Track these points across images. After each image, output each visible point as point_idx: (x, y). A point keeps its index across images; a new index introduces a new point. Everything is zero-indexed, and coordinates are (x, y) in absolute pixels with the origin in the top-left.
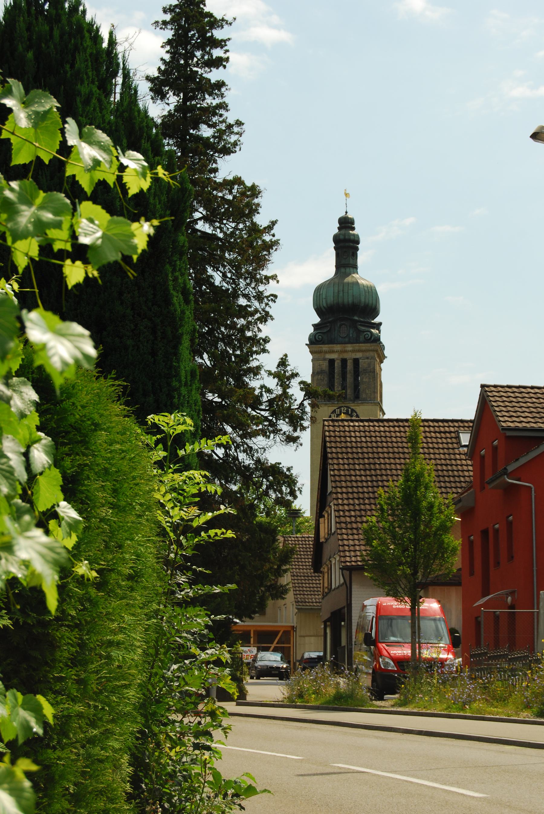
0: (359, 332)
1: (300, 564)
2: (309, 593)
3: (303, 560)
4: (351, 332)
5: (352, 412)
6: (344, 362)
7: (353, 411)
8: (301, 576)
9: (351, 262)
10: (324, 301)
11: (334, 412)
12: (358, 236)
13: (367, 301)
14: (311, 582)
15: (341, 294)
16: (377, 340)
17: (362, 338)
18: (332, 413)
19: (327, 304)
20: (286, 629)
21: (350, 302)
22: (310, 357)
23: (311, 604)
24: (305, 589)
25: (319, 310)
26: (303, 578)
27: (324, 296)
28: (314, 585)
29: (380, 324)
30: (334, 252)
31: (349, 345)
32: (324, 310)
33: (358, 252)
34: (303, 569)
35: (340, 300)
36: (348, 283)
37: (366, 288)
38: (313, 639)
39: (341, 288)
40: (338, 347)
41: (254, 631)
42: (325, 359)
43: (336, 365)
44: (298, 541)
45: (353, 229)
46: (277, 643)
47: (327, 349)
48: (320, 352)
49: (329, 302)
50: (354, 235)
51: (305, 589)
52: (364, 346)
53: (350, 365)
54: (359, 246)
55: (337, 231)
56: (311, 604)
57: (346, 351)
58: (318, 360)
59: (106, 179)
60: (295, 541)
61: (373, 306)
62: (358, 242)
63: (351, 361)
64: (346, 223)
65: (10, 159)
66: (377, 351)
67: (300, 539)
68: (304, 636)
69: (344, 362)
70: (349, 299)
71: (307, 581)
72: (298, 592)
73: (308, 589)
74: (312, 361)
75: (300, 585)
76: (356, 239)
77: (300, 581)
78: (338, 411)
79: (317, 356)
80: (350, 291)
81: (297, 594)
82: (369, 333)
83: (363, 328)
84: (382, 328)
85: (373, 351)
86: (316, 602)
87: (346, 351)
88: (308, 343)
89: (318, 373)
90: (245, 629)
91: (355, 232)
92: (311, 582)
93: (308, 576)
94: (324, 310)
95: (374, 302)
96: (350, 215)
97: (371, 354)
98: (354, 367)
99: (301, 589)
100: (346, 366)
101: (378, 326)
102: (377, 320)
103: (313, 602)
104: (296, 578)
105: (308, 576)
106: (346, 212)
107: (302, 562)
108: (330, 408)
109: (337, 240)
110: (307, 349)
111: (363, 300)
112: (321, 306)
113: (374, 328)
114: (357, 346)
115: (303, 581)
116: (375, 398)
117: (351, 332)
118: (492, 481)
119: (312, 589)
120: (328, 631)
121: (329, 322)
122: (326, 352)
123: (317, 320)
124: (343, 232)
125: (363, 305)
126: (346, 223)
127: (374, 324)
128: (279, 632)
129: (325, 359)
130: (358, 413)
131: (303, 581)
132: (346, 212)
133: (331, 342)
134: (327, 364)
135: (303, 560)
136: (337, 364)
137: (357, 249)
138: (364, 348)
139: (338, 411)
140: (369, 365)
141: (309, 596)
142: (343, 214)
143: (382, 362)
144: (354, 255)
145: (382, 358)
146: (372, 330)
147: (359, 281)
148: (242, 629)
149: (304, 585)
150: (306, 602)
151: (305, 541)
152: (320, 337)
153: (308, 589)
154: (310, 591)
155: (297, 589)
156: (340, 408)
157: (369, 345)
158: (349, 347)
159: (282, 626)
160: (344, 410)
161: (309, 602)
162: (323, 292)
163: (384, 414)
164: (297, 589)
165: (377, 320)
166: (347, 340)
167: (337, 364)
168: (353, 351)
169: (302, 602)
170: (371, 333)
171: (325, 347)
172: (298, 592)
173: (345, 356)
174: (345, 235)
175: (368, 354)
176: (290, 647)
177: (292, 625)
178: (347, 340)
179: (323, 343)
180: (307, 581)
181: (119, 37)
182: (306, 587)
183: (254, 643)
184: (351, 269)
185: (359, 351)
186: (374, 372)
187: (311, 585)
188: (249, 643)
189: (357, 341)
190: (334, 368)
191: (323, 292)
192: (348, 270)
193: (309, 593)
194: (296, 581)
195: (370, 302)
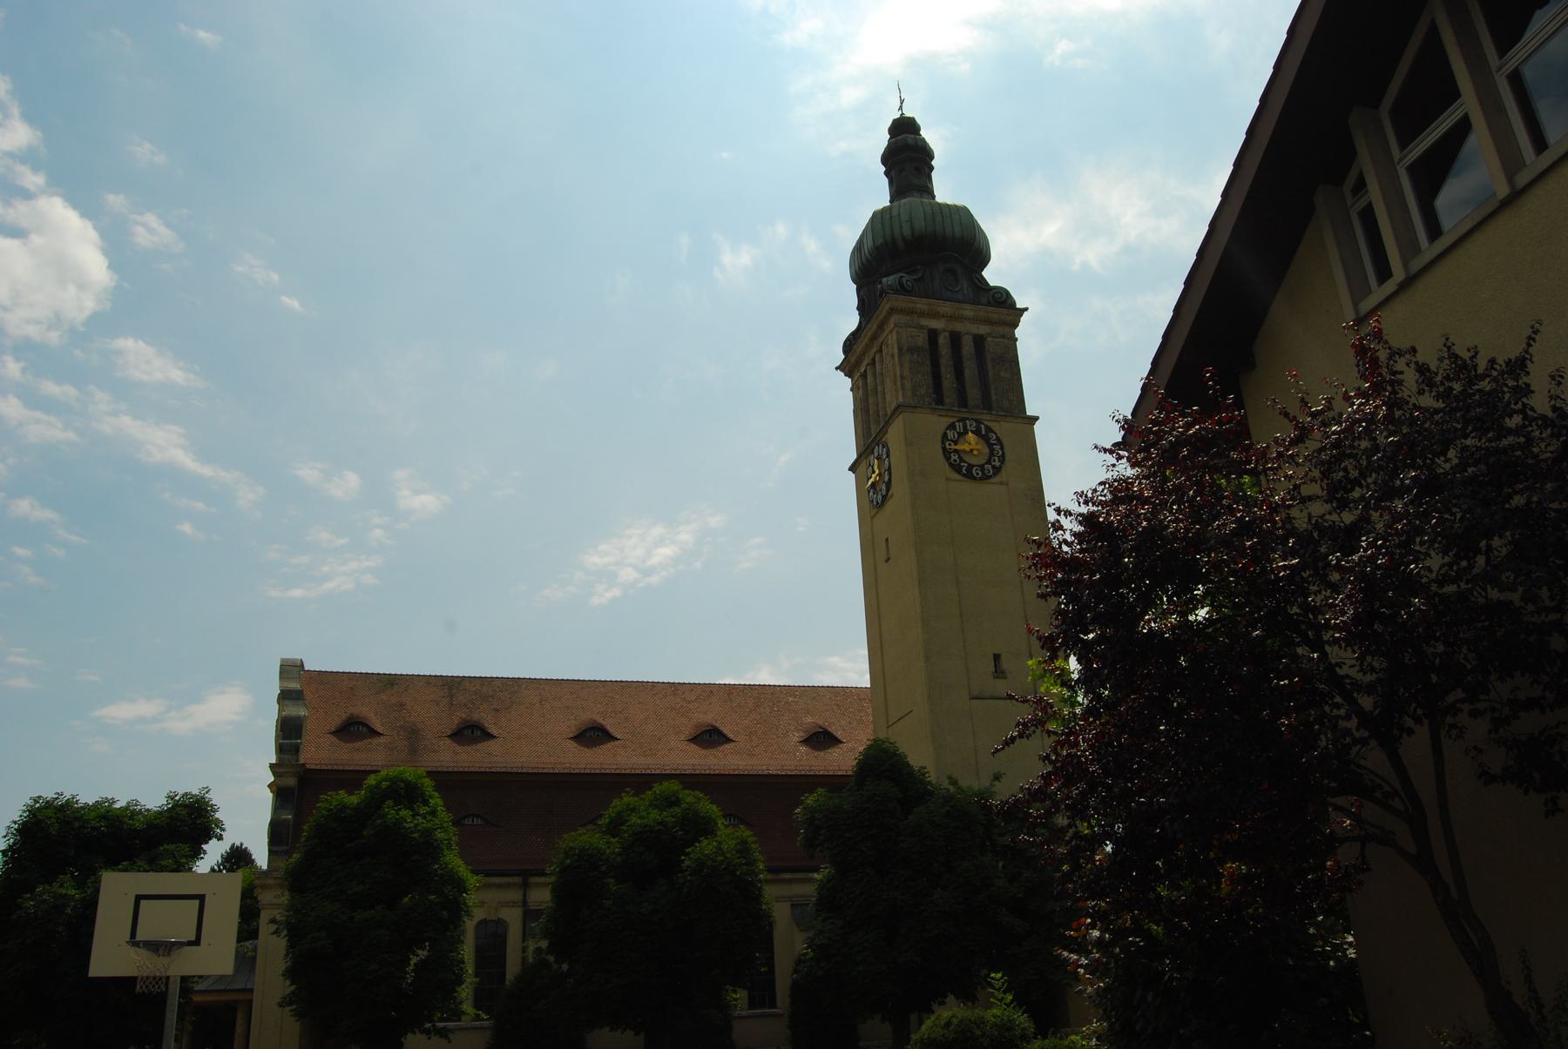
7: (989, 429)
11: (952, 426)
21: (958, 234)
22: (1018, 332)
40: (945, 308)
42: (922, 327)
53: (968, 348)
57: (961, 319)
87: (961, 319)
118: (1401, 160)
122: (922, 314)
156: (963, 420)
160: (971, 425)
163: (190, 821)
167: (943, 340)
168: (973, 320)
171: (922, 304)
173: (958, 327)
185: (991, 323)
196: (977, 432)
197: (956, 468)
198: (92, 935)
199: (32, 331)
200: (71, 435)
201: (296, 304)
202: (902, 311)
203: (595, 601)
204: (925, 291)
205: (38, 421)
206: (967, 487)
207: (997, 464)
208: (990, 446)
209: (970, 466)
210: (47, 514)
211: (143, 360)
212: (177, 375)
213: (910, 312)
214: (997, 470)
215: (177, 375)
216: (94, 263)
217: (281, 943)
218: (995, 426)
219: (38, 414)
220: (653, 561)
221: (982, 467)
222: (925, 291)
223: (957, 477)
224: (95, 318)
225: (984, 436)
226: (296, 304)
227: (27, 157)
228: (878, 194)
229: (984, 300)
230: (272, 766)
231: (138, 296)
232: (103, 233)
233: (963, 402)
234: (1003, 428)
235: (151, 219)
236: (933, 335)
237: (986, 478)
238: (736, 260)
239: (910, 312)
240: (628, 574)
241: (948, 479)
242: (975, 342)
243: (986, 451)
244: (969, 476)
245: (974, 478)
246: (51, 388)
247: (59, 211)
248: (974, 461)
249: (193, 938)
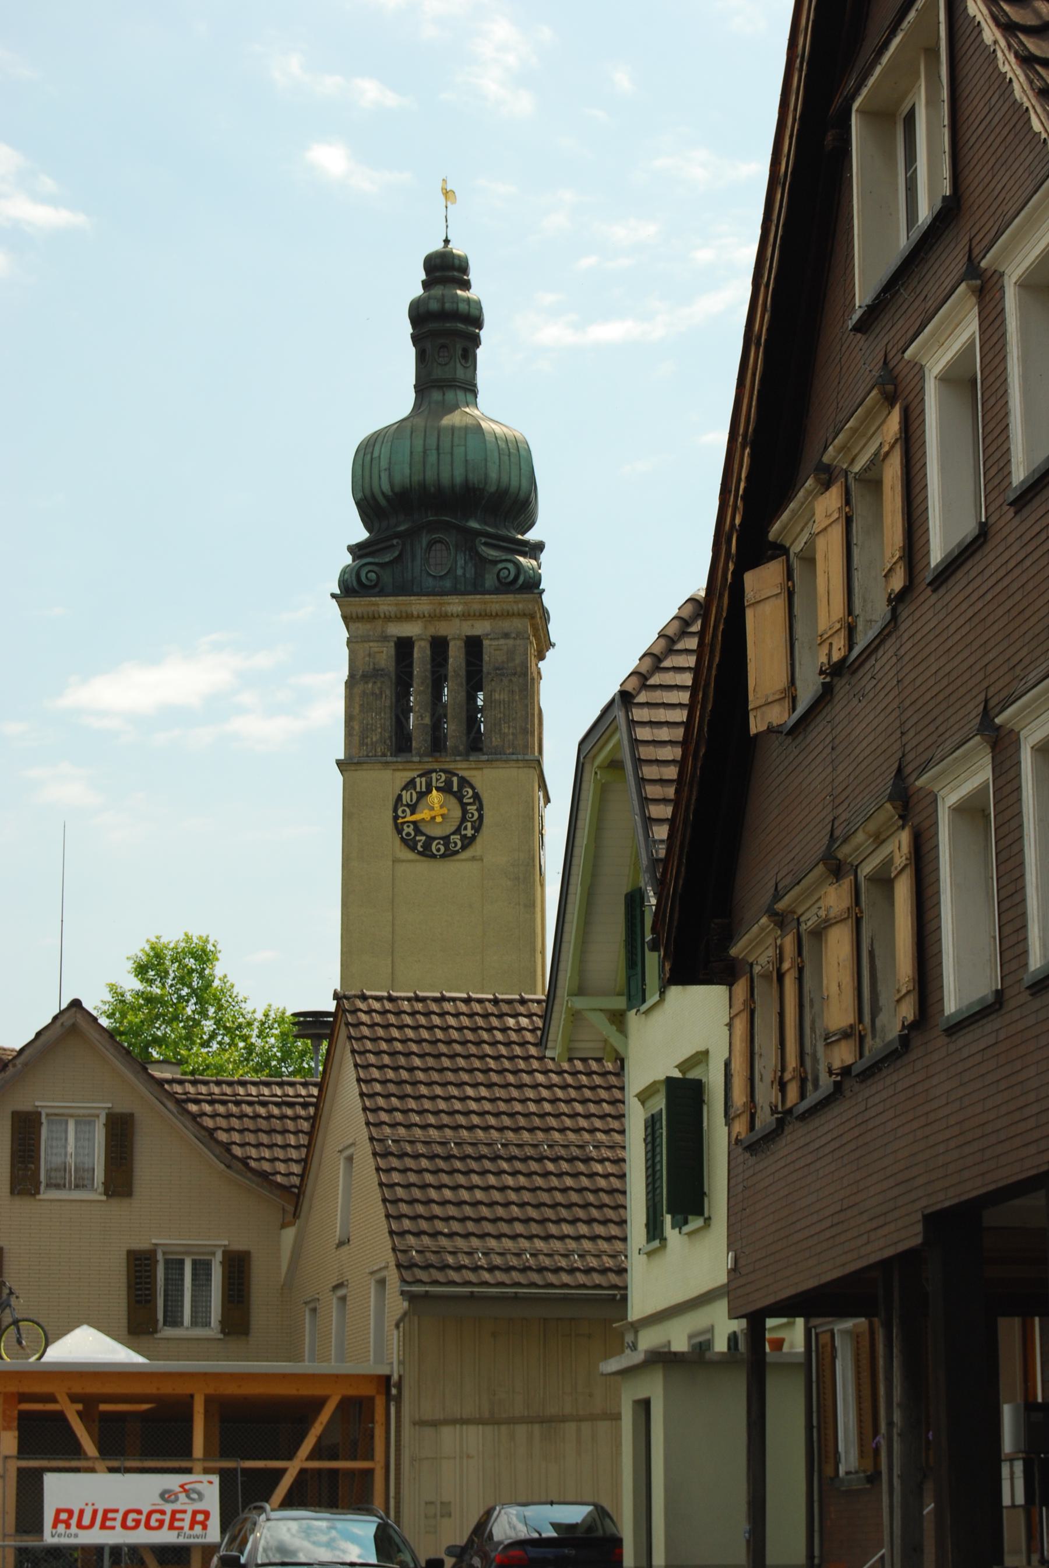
0: (483, 563)
1: (412, 1104)
2: (456, 1227)
3: (423, 1090)
4: (461, 562)
5: (461, 786)
6: (439, 646)
7: (464, 782)
8: (416, 1156)
9: (460, 373)
10: (384, 476)
11: (411, 784)
12: (478, 304)
13: (505, 479)
14: (461, 1179)
15: (432, 458)
16: (532, 585)
17: (490, 580)
18: (405, 788)
19: (392, 490)
20: (351, 1392)
21: (459, 480)
23: (471, 1276)
24: (437, 1210)
25: (369, 507)
26: (424, 1163)
27: (384, 464)
28: (479, 1195)
29: (539, 547)
30: (410, 353)
31: (455, 599)
32: (383, 502)
33: (480, 352)
34: (425, 1127)
35: (430, 475)
36: (453, 429)
37: (502, 445)
38: (473, 1435)
39: (432, 441)
40: (421, 605)
41: (209, 1400)
42: (385, 638)
43: (416, 654)
44: (398, 1013)
45: (466, 285)
46: (311, 1457)
47: (393, 609)
48: (373, 618)
49: (398, 478)
50: (468, 301)
51: (437, 1210)
52: (497, 602)
54: (483, 334)
55: (419, 291)
56: (471, 1276)
57: (445, 617)
58: (365, 639)
60: (384, 1013)
61: (522, 494)
62: (477, 322)
63: (460, 644)
64: (445, 270)
66: (532, 617)
67: (405, 1006)
68: (435, 1424)
69: (439, 646)
70: (452, 472)
71: (445, 1179)
72: (407, 1224)
73: (452, 1211)
74: (349, 642)
75: (417, 1193)
76: (474, 312)
77: (413, 1178)
78: (421, 783)
79: (362, 628)
80: (459, 451)
81: (402, 1234)
82: (510, 566)
83: (493, 553)
84: (544, 557)
85: (522, 615)
86: (492, 1269)
87: (445, 617)
88: (338, 591)
89: (366, 677)
90: (168, 1389)
91: (473, 293)
92: (461, 1179)
93: (448, 1158)
94: (383, 502)
95: (525, 483)
96: (457, 248)
97: (518, 624)
98: (469, 663)
99: (420, 1209)
100: (446, 659)
101: (536, 549)
102: (532, 536)
103: (476, 1269)
104: (395, 1162)
105: (448, 1158)
106: (447, 241)
107: (418, 1098)
108: (398, 774)
109: (421, 316)
110: (334, 610)
111: (493, 475)
112: (376, 490)
113: (524, 554)
114: (476, 602)
115: (429, 1178)
116: (527, 747)
117: (461, 562)
119: (468, 1210)
120: (145, 1407)
121: (398, 535)
122: (388, 619)
123: (361, 534)
124: (437, 291)
125: (492, 489)
126: (445, 270)
127: (526, 543)
128: (317, 1404)
130: (479, 790)
131: (429, 1178)
132: (447, 241)
133: (403, 589)
134: (392, 651)
135: (423, 1090)
136: (421, 653)
137: (476, 341)
138: (495, 608)
139: (421, 783)
140: (511, 653)
141: (460, 1242)
142: (438, 246)
143: (541, 657)
144: (469, 357)
145: (544, 644)
146: (521, 559)
147: (484, 424)
148: (150, 1389)
149: (433, 1194)
150: (446, 1267)
151: (428, 1014)
152: (372, 576)
153: (452, 1211)
154: (463, 1220)
155: (404, 1208)
156: (426, 774)
157: (510, 597)
158: (455, 605)
159: (337, 1378)
160: (438, 779)
161: (459, 1268)
162: (383, 452)
164: (404, 1208)
165: (532, 536)
166: (448, 584)
167: (421, 653)
168: (465, 616)
169: (427, 1267)
170: (518, 566)
171: (386, 605)
172: (407, 1224)
173: (443, 629)
174: (442, 300)
175: (506, 625)
176: (369, 1473)
177: (384, 1370)
178: (448, 584)
179: (382, 593)
180: (445, 1179)
182: (443, 1203)
183: (208, 1455)
184: (461, 395)
185: (484, 615)
186: (525, 674)
187: (465, 1195)
188: (186, 1452)
189: (476, 588)
190: (411, 665)
191: (383, 452)
192: (450, 395)
193: (456, 1227)
194: (396, 1177)
195: (514, 483)
196: (446, 789)
197: (410, 844)
198: (42, 1489)
206: (424, 868)
207: (469, 832)
208: (464, 806)
209: (430, 839)
214: (468, 842)
221: (446, 839)
223: (412, 856)
225: (457, 790)
228: (389, 389)
229: (490, 580)
230: (339, 763)
233: (437, 744)
234: (487, 779)
236: (404, 647)
237: (449, 854)
241: (396, 861)
242: (468, 653)
243: (457, 813)
244: (426, 853)
245: (434, 856)
248: (436, 832)
249: (9, 1460)
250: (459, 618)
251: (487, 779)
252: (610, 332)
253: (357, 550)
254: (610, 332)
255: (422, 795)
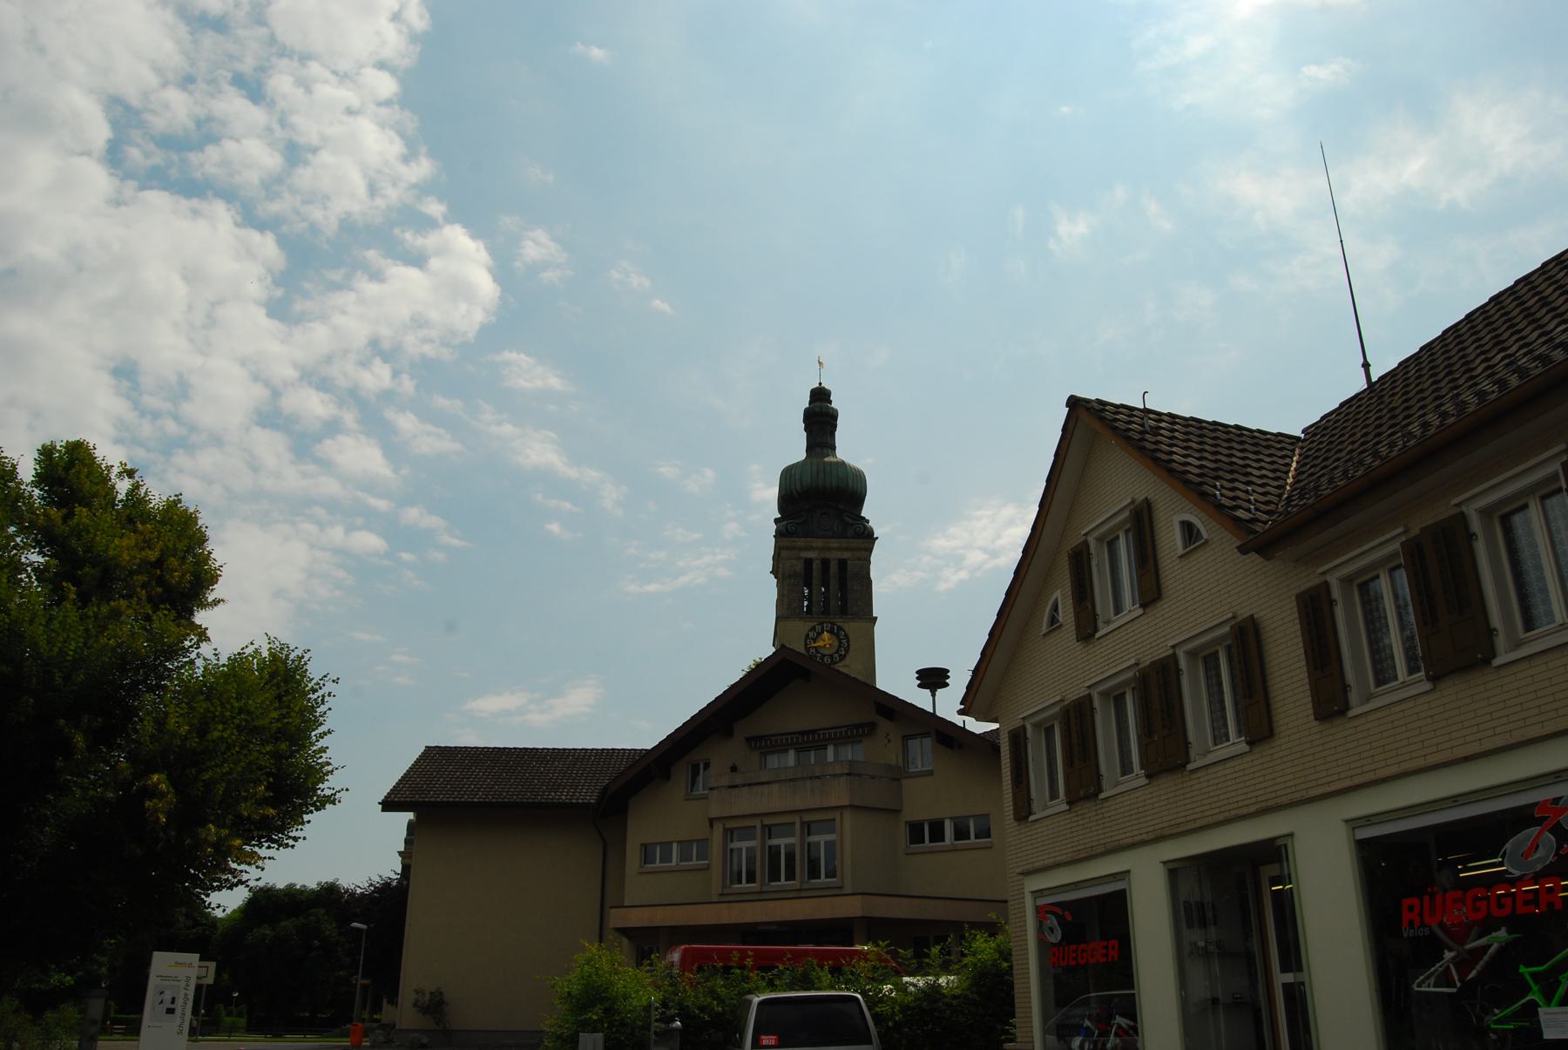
6: (825, 563)
7: (840, 628)
11: (813, 629)
40: (819, 543)
42: (799, 558)
57: (829, 549)
59: (1089, 392)
64: (820, 396)
65: (411, 827)
69: (825, 563)
78: (818, 628)
87: (829, 549)
126: (820, 396)
129: (799, 558)
133: (806, 535)
136: (816, 566)
156: (821, 624)
158: (834, 543)
160: (827, 626)
167: (816, 566)
168: (838, 549)
171: (801, 542)
173: (828, 555)
181: (330, 702)
185: (847, 549)
196: (831, 632)
199: (428, 349)
200: (458, 446)
201: (665, 307)
202: (787, 548)
203: (942, 586)
204: (823, 521)
205: (429, 434)
210: (433, 521)
211: (527, 373)
212: (554, 382)
213: (793, 548)
215: (554, 382)
216: (485, 284)
217: (858, 913)
218: (846, 626)
219: (430, 428)
220: (1002, 542)
222: (823, 521)
224: (485, 329)
226: (665, 307)
227: (424, 189)
228: (795, 449)
231: (522, 310)
232: (492, 250)
234: (851, 627)
235: (540, 235)
238: (1073, 230)
239: (793, 548)
240: (975, 557)
246: (441, 402)
247: (457, 236)
250: (836, 550)
251: (851, 627)
252: (652, 588)
253: (109, 141)
254: (652, 588)
255: (820, 634)
